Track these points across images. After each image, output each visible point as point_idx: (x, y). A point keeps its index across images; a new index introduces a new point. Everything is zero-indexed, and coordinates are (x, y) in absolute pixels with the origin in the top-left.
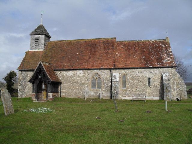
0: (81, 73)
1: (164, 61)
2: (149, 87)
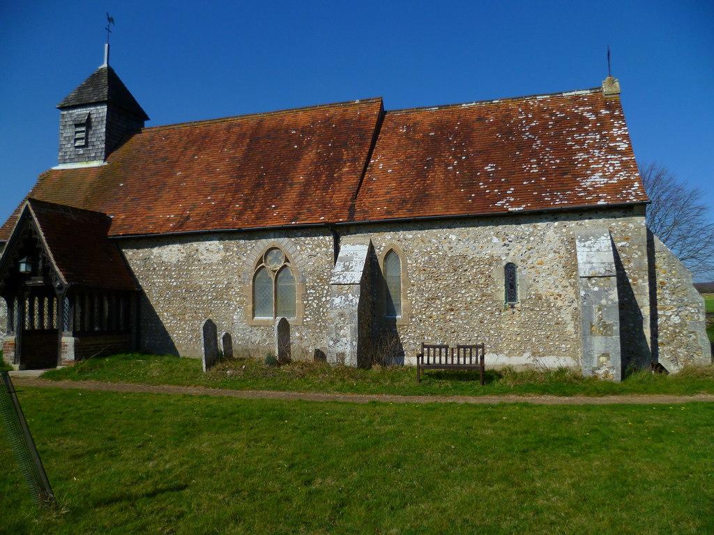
1: (587, 183)
2: (513, 307)
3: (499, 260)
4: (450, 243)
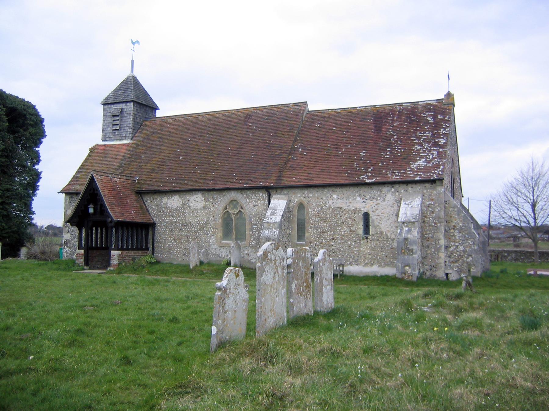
1: (414, 166)
2: (367, 238)
3: (360, 211)
4: (333, 200)
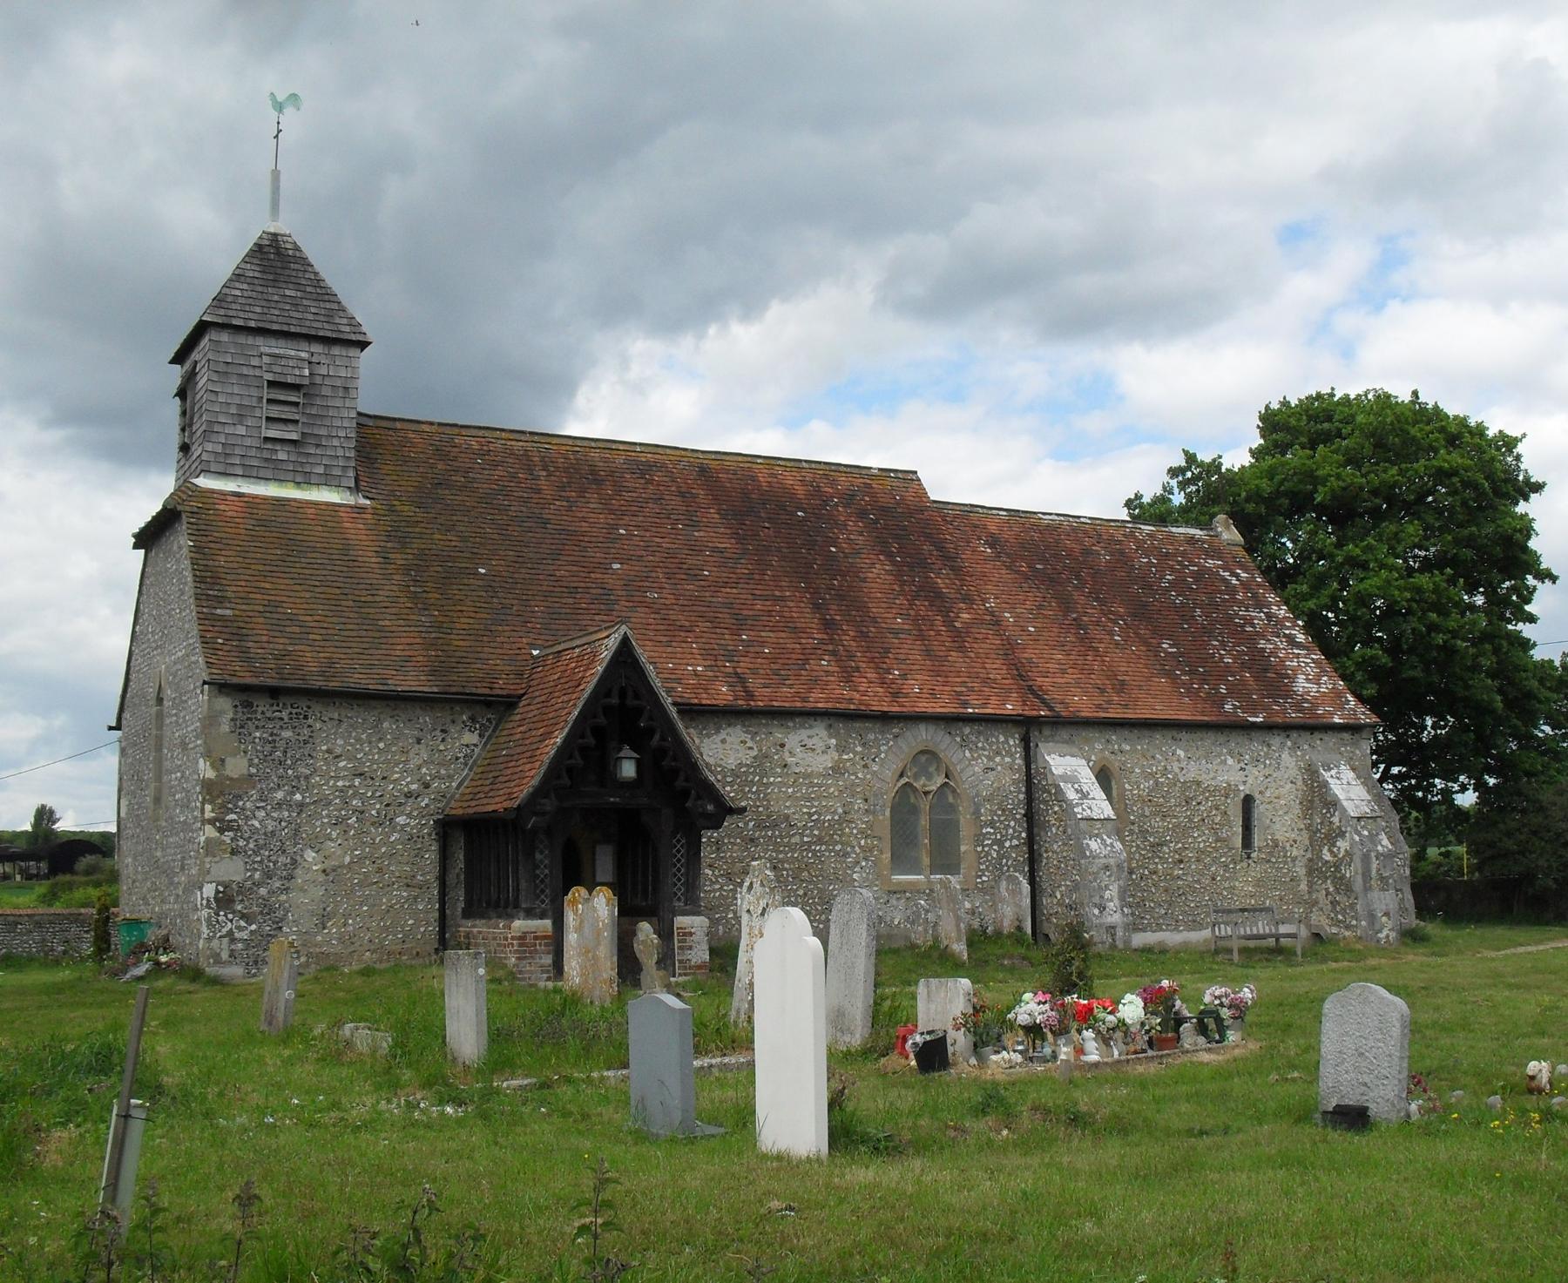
0: (820, 746)
2: (1249, 857)
